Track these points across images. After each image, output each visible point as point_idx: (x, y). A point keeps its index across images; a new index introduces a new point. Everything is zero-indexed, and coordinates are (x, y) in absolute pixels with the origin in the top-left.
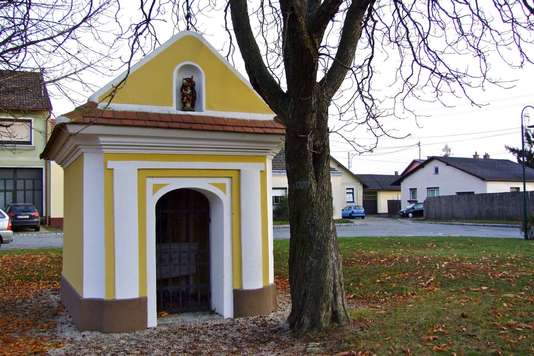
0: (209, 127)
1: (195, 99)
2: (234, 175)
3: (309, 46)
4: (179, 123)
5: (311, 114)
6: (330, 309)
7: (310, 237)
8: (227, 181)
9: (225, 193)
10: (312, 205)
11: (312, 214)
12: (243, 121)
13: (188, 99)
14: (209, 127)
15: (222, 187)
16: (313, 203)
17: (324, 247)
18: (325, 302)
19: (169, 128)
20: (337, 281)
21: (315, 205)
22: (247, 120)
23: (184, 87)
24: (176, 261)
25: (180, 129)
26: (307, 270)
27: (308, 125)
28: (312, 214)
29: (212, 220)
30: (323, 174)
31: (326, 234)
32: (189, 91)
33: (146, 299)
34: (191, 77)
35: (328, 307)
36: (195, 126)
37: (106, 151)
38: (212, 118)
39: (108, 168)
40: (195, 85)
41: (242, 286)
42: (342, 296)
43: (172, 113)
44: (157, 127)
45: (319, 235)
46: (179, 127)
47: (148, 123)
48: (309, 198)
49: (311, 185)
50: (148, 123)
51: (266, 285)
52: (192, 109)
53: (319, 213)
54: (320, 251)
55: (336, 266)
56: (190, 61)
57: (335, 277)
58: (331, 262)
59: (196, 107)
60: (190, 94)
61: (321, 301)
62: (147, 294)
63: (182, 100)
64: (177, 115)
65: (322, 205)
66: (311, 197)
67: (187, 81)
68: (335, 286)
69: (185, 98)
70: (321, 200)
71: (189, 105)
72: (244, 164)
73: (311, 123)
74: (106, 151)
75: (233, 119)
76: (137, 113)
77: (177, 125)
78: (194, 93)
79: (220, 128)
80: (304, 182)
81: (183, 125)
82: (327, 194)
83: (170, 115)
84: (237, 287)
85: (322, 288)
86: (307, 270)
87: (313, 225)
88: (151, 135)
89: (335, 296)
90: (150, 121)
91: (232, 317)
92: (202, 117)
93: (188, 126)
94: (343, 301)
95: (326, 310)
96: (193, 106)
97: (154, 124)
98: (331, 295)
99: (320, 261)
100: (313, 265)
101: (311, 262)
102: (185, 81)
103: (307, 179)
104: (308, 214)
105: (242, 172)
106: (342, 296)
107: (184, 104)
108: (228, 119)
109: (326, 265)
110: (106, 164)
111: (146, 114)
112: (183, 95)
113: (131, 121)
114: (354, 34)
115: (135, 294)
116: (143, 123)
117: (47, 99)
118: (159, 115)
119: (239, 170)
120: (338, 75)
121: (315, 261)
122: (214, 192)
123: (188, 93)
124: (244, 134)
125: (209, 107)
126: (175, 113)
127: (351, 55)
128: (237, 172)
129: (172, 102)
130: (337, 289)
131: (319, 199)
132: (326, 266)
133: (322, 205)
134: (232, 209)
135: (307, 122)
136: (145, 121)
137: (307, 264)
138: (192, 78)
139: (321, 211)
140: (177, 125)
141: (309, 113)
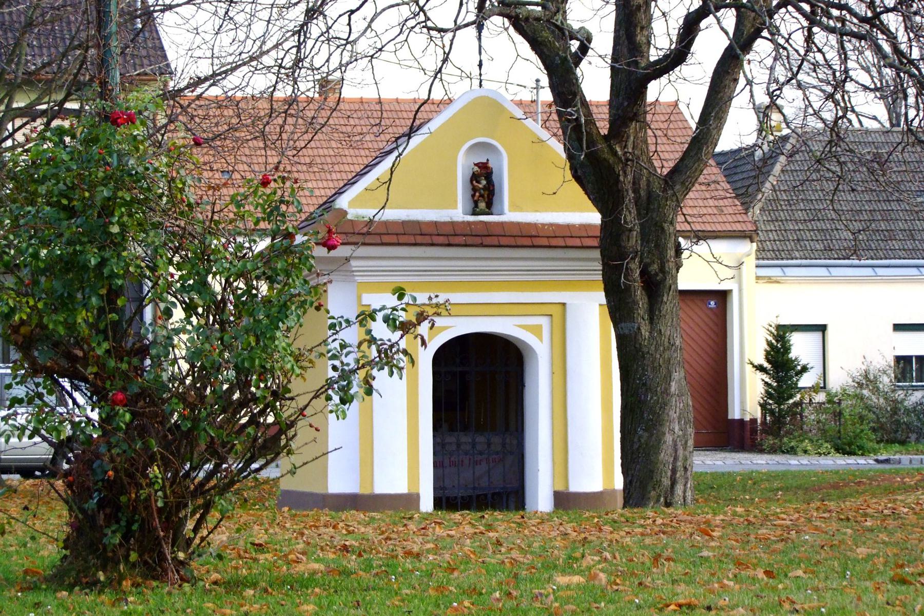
0: (511, 241)
1: (493, 195)
2: (556, 311)
3: (606, 156)
4: (464, 236)
5: (627, 233)
6: (662, 499)
7: (639, 402)
8: (544, 322)
9: (541, 340)
10: (643, 357)
11: (643, 369)
12: (569, 227)
13: (481, 196)
14: (511, 241)
15: (536, 330)
16: (643, 353)
17: (659, 416)
18: (654, 489)
19: (449, 245)
20: (679, 464)
21: (647, 356)
22: (574, 226)
23: (475, 177)
24: (468, 447)
25: (466, 245)
26: (636, 446)
27: (625, 247)
28: (643, 369)
29: (526, 385)
30: (660, 312)
31: (663, 398)
32: (484, 182)
33: (418, 496)
34: (485, 161)
35: (659, 496)
36: (487, 241)
37: (359, 279)
38: (519, 224)
39: (364, 303)
40: (492, 173)
41: (567, 487)
42: (685, 485)
43: (456, 219)
44: (432, 245)
45: (651, 398)
46: (463, 243)
47: (419, 239)
48: (637, 346)
49: (639, 329)
50: (419, 239)
51: (609, 488)
52: (489, 211)
53: (654, 368)
54: (652, 420)
55: (679, 443)
56: (482, 136)
57: (676, 459)
58: (669, 438)
59: (495, 208)
60: (485, 188)
61: (650, 488)
62: (418, 487)
63: (473, 196)
64: (463, 222)
65: (658, 356)
66: (640, 344)
67: (479, 167)
68: (674, 471)
69: (477, 194)
70: (656, 350)
71: (482, 205)
72: (572, 293)
73: (630, 244)
74: (359, 279)
75: (551, 225)
76: (404, 223)
77: (462, 240)
78: (490, 184)
79: (527, 242)
80: (629, 324)
81: (470, 240)
82: (667, 340)
83: (453, 224)
84: (560, 488)
85: (652, 471)
86: (636, 446)
87: (644, 384)
88: (424, 255)
89: (674, 483)
90: (421, 235)
91: (330, 287)
92: (502, 224)
93: (478, 240)
94: (685, 492)
95: (655, 500)
96: (489, 205)
97: (427, 239)
98: (666, 482)
99: (652, 435)
100: (643, 441)
101: (640, 437)
102: (476, 168)
103: (633, 320)
104: (637, 369)
105: (568, 306)
106: (685, 485)
107: (476, 203)
108: (543, 225)
109: (660, 440)
110: (359, 298)
111: (418, 223)
112: (475, 189)
113: (395, 237)
114: (721, 98)
115: (400, 487)
116: (412, 240)
117: (154, 48)
118: (436, 224)
119: (564, 304)
120: (691, 164)
121: (646, 435)
122: (523, 339)
123: (481, 186)
124: (565, 250)
125: (515, 207)
126: (460, 219)
127: (714, 132)
128: (559, 308)
129: (456, 201)
130: (678, 475)
131: (653, 348)
132: (659, 441)
133: (658, 356)
134: (552, 365)
135: (623, 244)
136: (414, 235)
137: (636, 440)
138: (487, 163)
139: (656, 364)
140: (462, 240)
141: (623, 232)
